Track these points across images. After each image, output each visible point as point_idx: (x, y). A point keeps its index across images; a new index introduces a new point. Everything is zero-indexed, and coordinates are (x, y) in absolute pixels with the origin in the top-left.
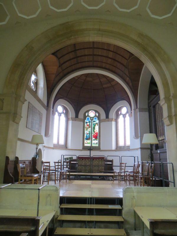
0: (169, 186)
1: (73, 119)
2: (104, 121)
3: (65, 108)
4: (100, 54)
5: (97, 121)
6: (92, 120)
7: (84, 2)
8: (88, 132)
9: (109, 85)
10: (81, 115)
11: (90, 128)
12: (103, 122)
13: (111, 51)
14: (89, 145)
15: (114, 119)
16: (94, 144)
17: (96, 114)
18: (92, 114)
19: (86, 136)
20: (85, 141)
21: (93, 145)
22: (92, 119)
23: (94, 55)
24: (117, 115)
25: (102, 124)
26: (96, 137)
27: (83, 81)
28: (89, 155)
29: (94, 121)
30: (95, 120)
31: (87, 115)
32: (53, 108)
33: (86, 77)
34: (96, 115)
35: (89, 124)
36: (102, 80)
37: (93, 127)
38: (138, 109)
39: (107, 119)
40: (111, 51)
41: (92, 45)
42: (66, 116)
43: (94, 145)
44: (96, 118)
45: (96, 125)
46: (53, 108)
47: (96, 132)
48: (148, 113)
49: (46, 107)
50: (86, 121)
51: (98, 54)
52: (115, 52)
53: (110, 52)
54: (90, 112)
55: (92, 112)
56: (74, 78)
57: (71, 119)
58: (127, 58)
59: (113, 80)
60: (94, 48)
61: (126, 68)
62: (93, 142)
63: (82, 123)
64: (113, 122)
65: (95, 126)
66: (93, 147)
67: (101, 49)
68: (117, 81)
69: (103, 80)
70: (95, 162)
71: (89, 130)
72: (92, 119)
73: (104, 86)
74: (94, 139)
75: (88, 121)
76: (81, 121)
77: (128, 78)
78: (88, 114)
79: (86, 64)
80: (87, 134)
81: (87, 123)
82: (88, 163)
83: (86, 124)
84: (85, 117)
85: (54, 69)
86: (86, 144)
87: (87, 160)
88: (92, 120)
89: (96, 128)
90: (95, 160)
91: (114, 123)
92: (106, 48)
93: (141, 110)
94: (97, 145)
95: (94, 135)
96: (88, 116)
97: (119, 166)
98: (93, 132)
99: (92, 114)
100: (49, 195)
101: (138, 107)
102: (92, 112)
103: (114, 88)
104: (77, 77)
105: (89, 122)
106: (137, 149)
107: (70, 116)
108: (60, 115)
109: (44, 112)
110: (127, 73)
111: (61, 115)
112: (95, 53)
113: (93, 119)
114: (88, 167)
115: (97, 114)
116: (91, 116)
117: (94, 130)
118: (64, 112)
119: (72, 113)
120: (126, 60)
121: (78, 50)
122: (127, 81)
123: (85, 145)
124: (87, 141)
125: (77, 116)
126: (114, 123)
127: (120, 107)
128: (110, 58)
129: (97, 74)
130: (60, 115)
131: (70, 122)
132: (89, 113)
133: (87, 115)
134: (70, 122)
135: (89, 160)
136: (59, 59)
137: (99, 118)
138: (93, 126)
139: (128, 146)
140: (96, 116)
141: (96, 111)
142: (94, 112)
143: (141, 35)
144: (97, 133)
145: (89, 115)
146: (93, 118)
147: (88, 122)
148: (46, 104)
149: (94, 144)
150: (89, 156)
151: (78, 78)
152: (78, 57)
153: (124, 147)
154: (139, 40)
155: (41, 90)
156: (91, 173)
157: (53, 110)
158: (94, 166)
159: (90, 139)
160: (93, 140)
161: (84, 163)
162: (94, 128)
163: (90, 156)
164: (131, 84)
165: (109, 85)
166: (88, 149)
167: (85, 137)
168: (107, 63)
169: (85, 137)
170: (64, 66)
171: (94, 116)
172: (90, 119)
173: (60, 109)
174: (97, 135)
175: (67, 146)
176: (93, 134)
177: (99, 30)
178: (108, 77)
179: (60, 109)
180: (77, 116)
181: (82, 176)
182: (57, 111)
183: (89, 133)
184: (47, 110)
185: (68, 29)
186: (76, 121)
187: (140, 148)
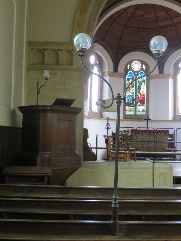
0: (174, 177)
1: (110, 75)
2: (155, 77)
6: (136, 76)
8: (130, 94)
9: (168, 23)
10: (121, 69)
11: (133, 88)
12: (153, 78)
14: (133, 113)
17: (142, 66)
18: (136, 66)
19: (128, 100)
21: (138, 113)
22: (136, 73)
25: (152, 82)
26: (142, 102)
27: (130, 15)
28: (146, 127)
31: (128, 68)
34: (143, 69)
37: (137, 87)
39: (161, 75)
42: (100, 70)
43: (140, 112)
45: (143, 83)
47: (142, 94)
50: (127, 77)
54: (134, 62)
55: (136, 63)
56: (118, 11)
57: (107, 74)
62: (138, 108)
63: (122, 80)
66: (138, 115)
68: (177, 12)
70: (159, 137)
72: (136, 73)
73: (160, 24)
74: (139, 104)
75: (130, 77)
76: (122, 78)
78: (130, 66)
80: (130, 96)
81: (129, 79)
82: (146, 137)
83: (127, 82)
84: (126, 71)
86: (128, 111)
87: (144, 134)
88: (136, 76)
89: (142, 87)
90: (140, 134)
94: (144, 113)
96: (130, 69)
97: (178, 142)
99: (136, 66)
100: (162, 173)
102: (136, 63)
106: (116, 111)
113: (138, 74)
114: (146, 143)
115: (144, 67)
116: (134, 70)
117: (139, 91)
123: (127, 113)
125: (116, 70)
126: (171, 81)
132: (132, 64)
133: (128, 68)
135: (148, 134)
138: (138, 85)
140: (142, 69)
141: (143, 62)
142: (139, 63)
144: (143, 95)
146: (138, 72)
147: (131, 78)
149: (139, 111)
150: (146, 129)
156: (154, 151)
158: (139, 141)
161: (140, 137)
162: (140, 87)
163: (147, 128)
165: (168, 23)
166: (145, 119)
171: (139, 69)
172: (133, 75)
174: (144, 98)
175: (102, 115)
178: (171, 10)
180: (116, 70)
183: (132, 96)
186: (115, 76)
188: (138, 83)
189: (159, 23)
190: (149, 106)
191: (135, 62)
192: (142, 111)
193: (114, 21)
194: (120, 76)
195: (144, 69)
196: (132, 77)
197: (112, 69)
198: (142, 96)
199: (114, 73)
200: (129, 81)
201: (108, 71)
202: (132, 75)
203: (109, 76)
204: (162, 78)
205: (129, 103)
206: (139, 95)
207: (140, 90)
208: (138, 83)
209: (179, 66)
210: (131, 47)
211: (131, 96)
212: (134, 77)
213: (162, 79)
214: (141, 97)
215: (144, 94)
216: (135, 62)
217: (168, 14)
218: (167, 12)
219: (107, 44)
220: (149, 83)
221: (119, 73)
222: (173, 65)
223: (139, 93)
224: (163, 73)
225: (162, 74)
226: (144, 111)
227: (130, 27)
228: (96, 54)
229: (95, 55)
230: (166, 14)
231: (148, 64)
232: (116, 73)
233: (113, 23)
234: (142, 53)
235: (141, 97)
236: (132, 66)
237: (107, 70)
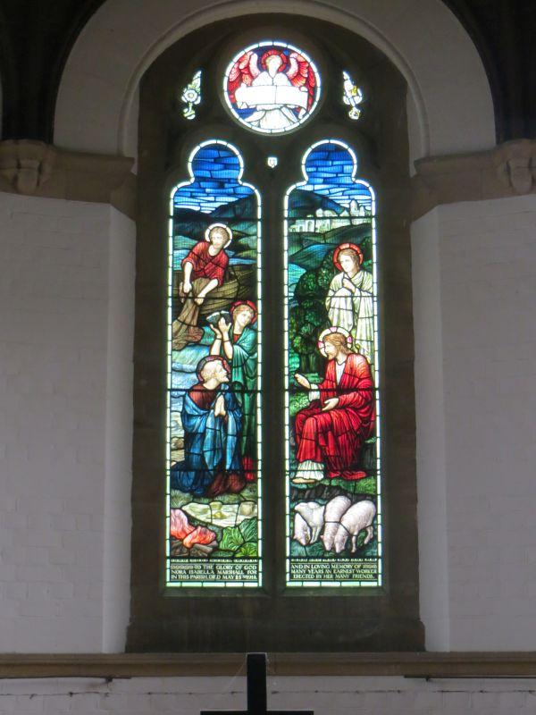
2: (463, 179)
6: (272, 183)
8: (215, 374)
17: (333, 90)
19: (191, 437)
25: (277, 111)
29: (309, 204)
35: (237, 247)
50: (179, 199)
62: (306, 519)
63: (114, 230)
65: (321, 268)
66: (302, 599)
81: (192, 223)
83: (177, 252)
84: (165, 140)
88: (272, 183)
95: (317, 406)
96: (214, 115)
98: (290, 362)
102: (274, 62)
105: (236, 214)
113: (289, 171)
115: (352, 95)
117: (311, 342)
133: (189, 114)
137: (380, 145)
138: (291, 275)
140: (329, 114)
146: (288, 146)
162: (312, 304)
167: (173, 456)
176: (290, 406)
194: (84, 179)
195: (354, 114)
198: (339, 390)
202: (225, 174)
212: (252, 197)
221: (61, 151)
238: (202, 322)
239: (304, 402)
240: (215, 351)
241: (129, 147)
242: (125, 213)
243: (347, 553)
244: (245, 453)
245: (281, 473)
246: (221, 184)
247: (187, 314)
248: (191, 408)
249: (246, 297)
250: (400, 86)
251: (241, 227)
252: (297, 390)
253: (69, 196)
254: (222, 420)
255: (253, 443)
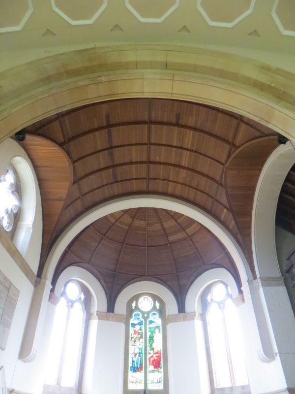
1: (100, 316)
2: (174, 319)
3: (85, 290)
4: (162, 161)
5: (158, 321)
6: (146, 319)
7: (130, 2)
8: (137, 351)
9: (181, 235)
11: (141, 340)
13: (187, 149)
15: (197, 314)
16: (153, 382)
17: (155, 304)
18: (146, 304)
19: (133, 362)
20: (131, 374)
21: (151, 387)
22: (146, 315)
23: (150, 162)
24: (204, 304)
25: (169, 327)
29: (151, 322)
30: (153, 320)
31: (133, 308)
32: (54, 283)
33: (133, 218)
34: (156, 307)
35: (140, 329)
36: (166, 225)
38: (259, 280)
40: (187, 149)
41: (146, 138)
42: (85, 309)
44: (154, 314)
45: (157, 330)
46: (54, 283)
47: (155, 351)
48: (285, 287)
49: (35, 278)
50: (132, 321)
51: (157, 159)
52: (195, 152)
53: (185, 151)
55: (146, 299)
56: (105, 218)
58: (223, 161)
59: (192, 221)
60: (151, 144)
61: (221, 184)
62: (150, 376)
63: (123, 326)
64: (195, 320)
65: (153, 332)
66: (150, 391)
67: (164, 145)
69: (169, 224)
71: (141, 343)
73: (171, 238)
75: (136, 322)
76: (121, 321)
77: (225, 210)
79: (135, 186)
80: (135, 355)
81: (134, 325)
83: (131, 330)
84: (130, 311)
85: (62, 189)
88: (146, 319)
91: (198, 323)
92: (175, 145)
93: (267, 282)
94: (160, 387)
95: (152, 356)
96: (137, 308)
98: (148, 348)
99: (146, 304)
101: (258, 275)
102: (146, 299)
103: (192, 242)
104: (112, 215)
105: (140, 324)
107: (95, 309)
108: (71, 304)
109: (25, 288)
110: (224, 199)
111: (72, 306)
112: (152, 159)
113: (148, 317)
115: (158, 305)
117: (151, 345)
118: (80, 299)
119: (99, 301)
120: (222, 166)
121: (118, 147)
122: (222, 219)
124: (135, 374)
125: (111, 308)
126: (198, 323)
127: (213, 283)
128: (184, 168)
129: (155, 210)
130: (71, 304)
131: (95, 323)
133: (133, 308)
134: (95, 323)
136: (74, 162)
137: (162, 312)
138: (149, 334)
139: (243, 387)
140: (154, 308)
141: (155, 298)
142: (150, 298)
143: (265, 69)
145: (140, 306)
146: (148, 313)
148: (35, 269)
151: (117, 220)
152: (117, 165)
153: (231, 388)
154: (263, 78)
155: (26, 233)
157: (51, 287)
159: (141, 368)
160: (150, 372)
162: (151, 338)
164: (232, 224)
165: (181, 235)
167: (130, 365)
168: (177, 182)
169: (130, 365)
170: (86, 184)
172: (141, 317)
173: (73, 290)
174: (159, 357)
176: (148, 356)
177: (166, 66)
178: (181, 215)
179: (73, 290)
180: (111, 308)
181: (145, 366)
182: (63, 294)
184: (35, 286)
185: (95, 65)
186: (108, 320)
187: (287, 388)
188: (149, 331)
189: (169, 238)
190: (168, 373)
191: (144, 298)
192: (156, 382)
193: (104, 235)
194: (119, 319)
195: (158, 308)
196: (139, 321)
197: (104, 307)
198: (156, 353)
199: (108, 313)
200: (134, 327)
201: (97, 311)
202: (138, 317)
203: (99, 319)
204: (184, 320)
205: (134, 367)
206: (150, 351)
207: (153, 343)
208: (149, 331)
209: (207, 300)
210: (135, 274)
211: (138, 355)
212: (142, 321)
213: (184, 322)
214: (155, 355)
215: (159, 350)
216: (144, 298)
217: (178, 223)
218: (176, 220)
219: (97, 269)
220: (166, 330)
221: (115, 314)
222: (199, 298)
223: (151, 348)
224: (185, 312)
225: (182, 312)
226: (160, 382)
227: (130, 245)
228: (80, 284)
229: (79, 285)
230: (175, 223)
231: (160, 298)
232: (111, 314)
233: (102, 238)
234: (152, 282)
235: (155, 355)
236: (140, 303)
237: (96, 310)
238: (135, 342)
239: (151, 355)
240: (137, 347)
241: (125, 314)
242: (90, 304)
243: (158, 383)
244: (141, 365)
245: (147, 368)
246: (138, 319)
247: (133, 340)
248: (133, 357)
249: (141, 337)
250: (164, 304)
251: (141, 326)
252: (149, 353)
253: (116, 321)
254: (138, 359)
255: (142, 363)
